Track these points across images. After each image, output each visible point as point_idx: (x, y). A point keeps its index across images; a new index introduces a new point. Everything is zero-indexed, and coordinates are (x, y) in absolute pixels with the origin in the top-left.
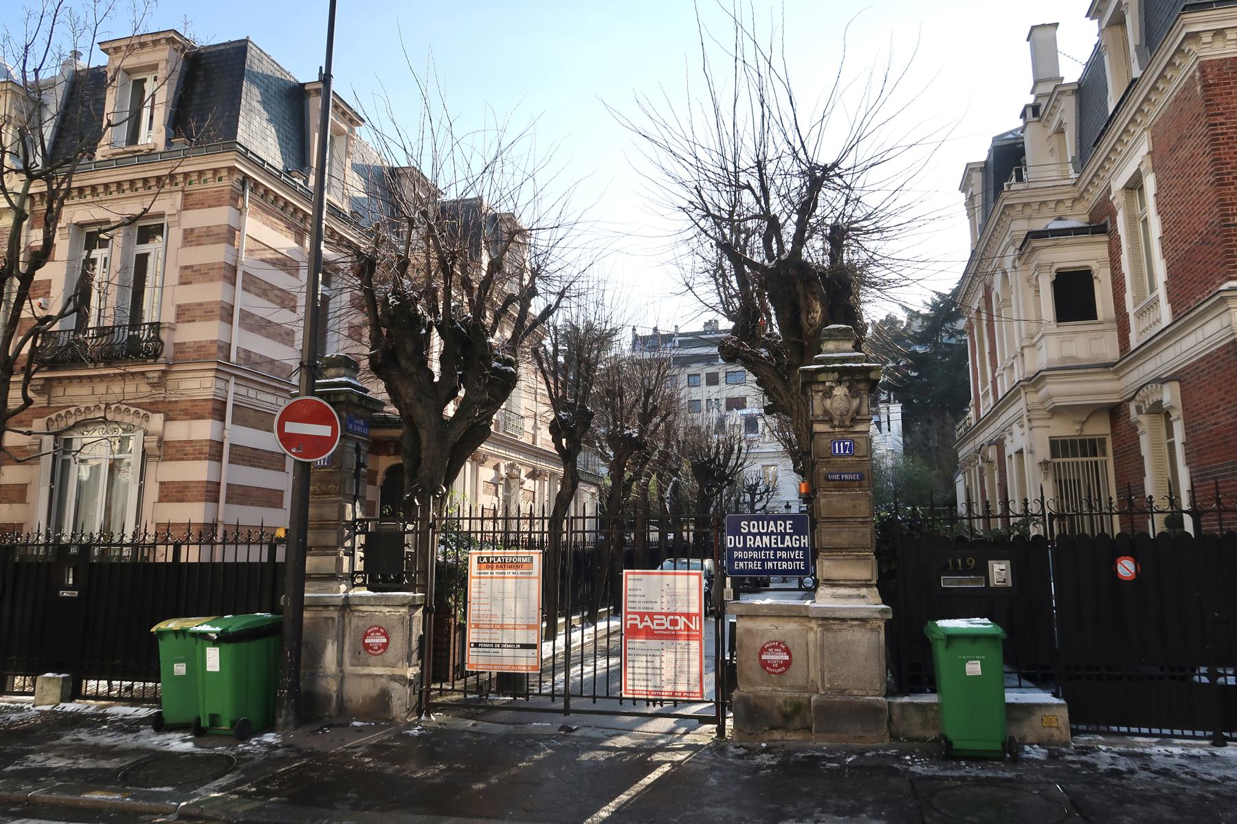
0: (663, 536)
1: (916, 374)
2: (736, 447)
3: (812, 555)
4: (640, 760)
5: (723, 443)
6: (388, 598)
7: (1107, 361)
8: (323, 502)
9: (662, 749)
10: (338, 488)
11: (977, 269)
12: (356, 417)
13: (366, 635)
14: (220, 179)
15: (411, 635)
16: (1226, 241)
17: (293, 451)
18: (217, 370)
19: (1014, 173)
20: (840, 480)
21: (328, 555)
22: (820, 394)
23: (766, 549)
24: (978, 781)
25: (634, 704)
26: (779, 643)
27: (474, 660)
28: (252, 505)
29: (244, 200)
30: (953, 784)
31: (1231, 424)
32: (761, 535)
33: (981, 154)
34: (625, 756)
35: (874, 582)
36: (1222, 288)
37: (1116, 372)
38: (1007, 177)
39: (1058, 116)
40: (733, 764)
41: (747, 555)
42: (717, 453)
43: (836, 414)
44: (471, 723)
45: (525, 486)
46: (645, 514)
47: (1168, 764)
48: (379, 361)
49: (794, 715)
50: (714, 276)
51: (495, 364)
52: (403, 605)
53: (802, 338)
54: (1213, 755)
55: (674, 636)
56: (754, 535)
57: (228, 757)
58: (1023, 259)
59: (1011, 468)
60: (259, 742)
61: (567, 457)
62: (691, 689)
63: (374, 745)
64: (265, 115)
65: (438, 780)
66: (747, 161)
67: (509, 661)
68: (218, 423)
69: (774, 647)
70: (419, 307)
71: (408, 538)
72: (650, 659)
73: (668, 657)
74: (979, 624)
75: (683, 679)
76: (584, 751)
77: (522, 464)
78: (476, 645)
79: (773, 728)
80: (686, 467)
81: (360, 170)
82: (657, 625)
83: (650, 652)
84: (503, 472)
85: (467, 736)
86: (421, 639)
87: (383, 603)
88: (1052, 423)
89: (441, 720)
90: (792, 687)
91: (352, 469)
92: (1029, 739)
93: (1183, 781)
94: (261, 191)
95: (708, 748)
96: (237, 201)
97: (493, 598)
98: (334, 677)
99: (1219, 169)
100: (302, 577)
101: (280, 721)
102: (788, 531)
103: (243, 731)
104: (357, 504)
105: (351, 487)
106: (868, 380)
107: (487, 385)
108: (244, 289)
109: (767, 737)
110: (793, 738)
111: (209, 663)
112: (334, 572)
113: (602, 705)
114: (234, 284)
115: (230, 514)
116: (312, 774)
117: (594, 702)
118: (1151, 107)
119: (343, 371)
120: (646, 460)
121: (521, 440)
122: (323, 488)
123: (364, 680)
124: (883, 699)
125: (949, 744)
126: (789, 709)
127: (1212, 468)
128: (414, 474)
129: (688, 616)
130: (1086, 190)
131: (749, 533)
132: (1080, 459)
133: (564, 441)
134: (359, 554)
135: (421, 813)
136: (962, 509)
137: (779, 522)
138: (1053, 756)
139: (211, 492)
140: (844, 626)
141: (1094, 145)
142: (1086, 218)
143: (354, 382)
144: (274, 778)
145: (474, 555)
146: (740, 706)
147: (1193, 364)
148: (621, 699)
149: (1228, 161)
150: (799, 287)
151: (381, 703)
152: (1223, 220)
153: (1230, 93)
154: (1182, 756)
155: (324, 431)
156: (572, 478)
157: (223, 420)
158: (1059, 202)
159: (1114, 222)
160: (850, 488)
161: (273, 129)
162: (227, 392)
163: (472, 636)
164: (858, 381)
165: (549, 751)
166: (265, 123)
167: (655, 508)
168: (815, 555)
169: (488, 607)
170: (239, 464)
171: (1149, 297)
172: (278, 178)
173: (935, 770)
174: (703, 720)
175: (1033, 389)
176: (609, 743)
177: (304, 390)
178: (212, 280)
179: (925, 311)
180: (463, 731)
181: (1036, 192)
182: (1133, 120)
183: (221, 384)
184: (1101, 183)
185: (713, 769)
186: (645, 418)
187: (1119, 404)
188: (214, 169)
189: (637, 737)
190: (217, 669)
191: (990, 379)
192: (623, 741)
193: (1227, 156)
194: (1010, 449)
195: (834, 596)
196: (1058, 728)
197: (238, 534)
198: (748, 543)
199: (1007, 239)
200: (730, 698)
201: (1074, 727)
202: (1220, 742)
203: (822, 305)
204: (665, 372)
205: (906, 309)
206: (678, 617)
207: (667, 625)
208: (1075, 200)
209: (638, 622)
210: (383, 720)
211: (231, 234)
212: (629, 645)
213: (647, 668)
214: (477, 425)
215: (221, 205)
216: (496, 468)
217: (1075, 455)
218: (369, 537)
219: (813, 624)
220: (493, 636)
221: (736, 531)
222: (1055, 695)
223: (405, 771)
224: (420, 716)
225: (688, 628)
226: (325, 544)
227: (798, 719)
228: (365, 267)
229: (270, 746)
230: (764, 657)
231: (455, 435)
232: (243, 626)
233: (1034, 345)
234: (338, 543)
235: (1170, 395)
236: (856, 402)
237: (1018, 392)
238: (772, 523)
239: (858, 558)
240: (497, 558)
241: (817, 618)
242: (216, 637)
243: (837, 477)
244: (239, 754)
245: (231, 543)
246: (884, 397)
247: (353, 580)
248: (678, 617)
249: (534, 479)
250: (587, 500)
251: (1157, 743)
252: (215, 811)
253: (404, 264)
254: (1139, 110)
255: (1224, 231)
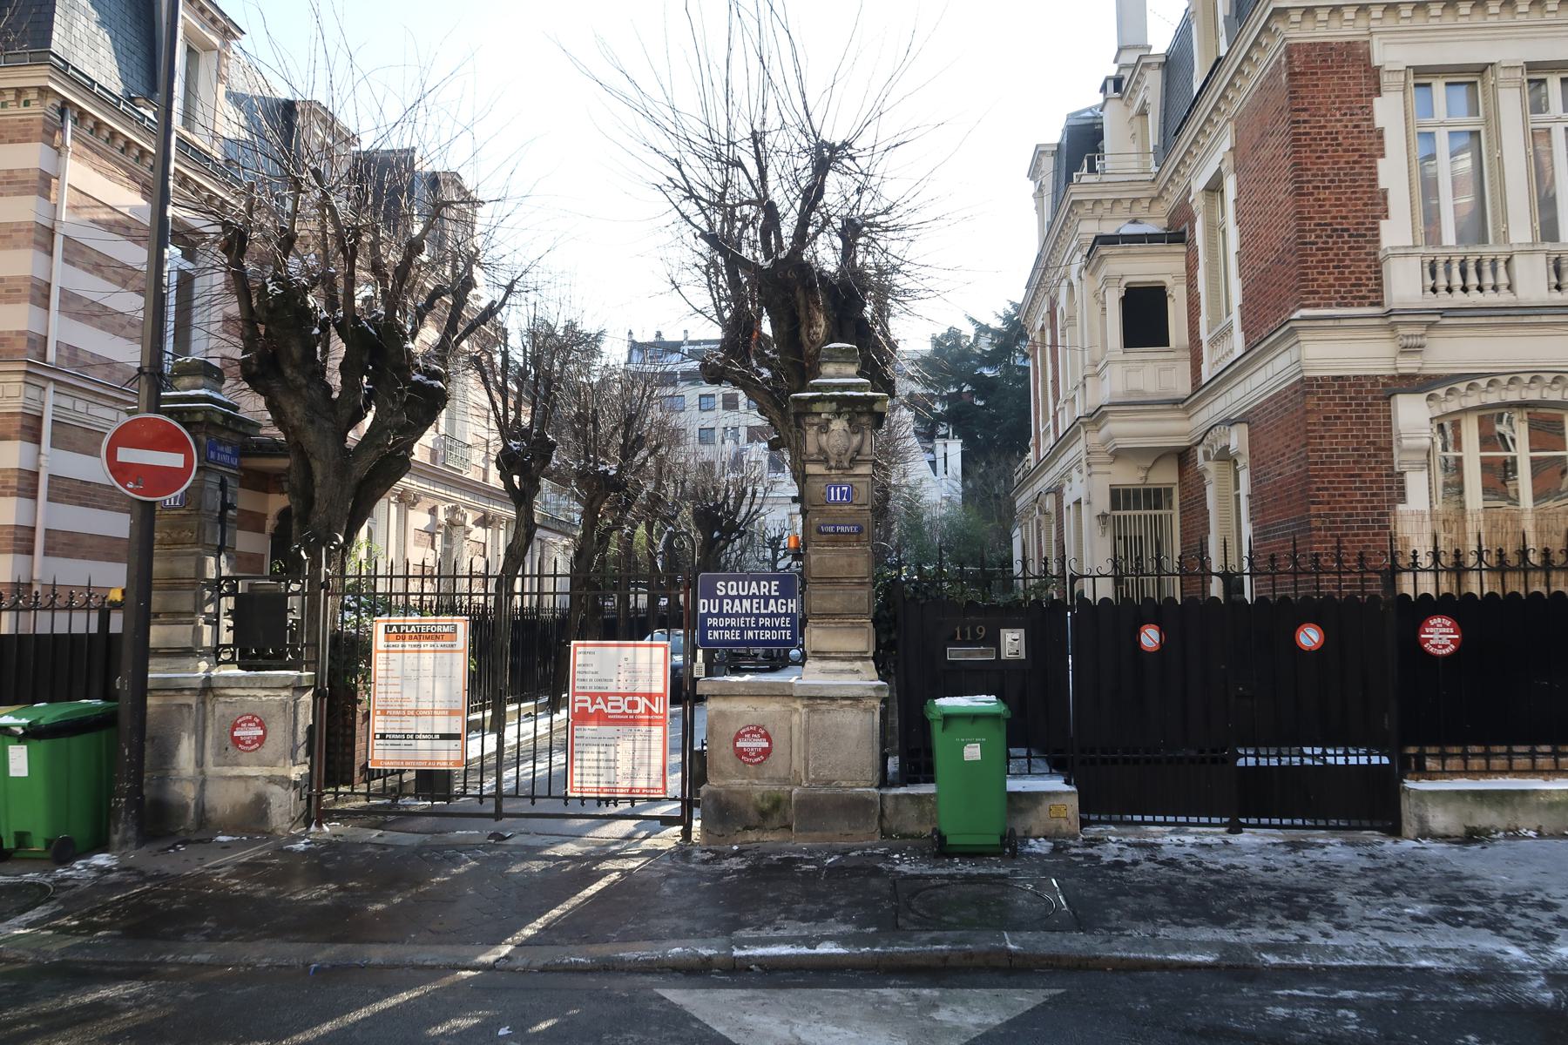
0: (653, 600)
1: (982, 403)
2: (750, 490)
3: (800, 624)
4: (584, 870)
5: (733, 484)
6: (265, 678)
7: (1177, 397)
8: (177, 555)
9: (614, 856)
10: (195, 536)
11: (1042, 278)
12: (220, 442)
13: (235, 726)
14: (27, 103)
15: (296, 725)
16: (1300, 262)
17: (130, 485)
18: (27, 373)
19: (1085, 161)
20: (835, 532)
21: (181, 623)
22: (815, 428)
23: (747, 615)
24: (969, 879)
25: (583, 804)
26: (758, 728)
27: (381, 755)
28: (84, 558)
29: (64, 135)
30: (939, 882)
31: (1295, 475)
32: (741, 598)
33: (1054, 135)
34: (567, 865)
35: (871, 654)
36: (1294, 316)
37: (1186, 410)
38: (1078, 167)
39: (1141, 95)
40: (693, 870)
41: (723, 622)
42: (727, 497)
43: (833, 453)
44: (376, 833)
45: (472, 536)
46: (629, 571)
47: (1177, 853)
48: (254, 368)
49: (772, 812)
50: (707, 273)
51: (417, 377)
52: (285, 687)
53: (801, 357)
54: (1226, 843)
55: (634, 721)
56: (733, 598)
57: (41, 886)
58: (1090, 268)
59: (1069, 518)
60: (86, 866)
61: (522, 499)
62: (652, 784)
63: (244, 864)
64: (95, 15)
65: (325, 902)
66: (742, 131)
67: (426, 756)
68: (31, 447)
69: (751, 732)
70: (310, 298)
71: (293, 602)
72: (602, 749)
73: (625, 747)
74: (984, 702)
75: (643, 773)
76: (516, 863)
77: (467, 507)
78: (383, 736)
79: (747, 828)
80: (686, 514)
81: (237, 99)
82: (612, 707)
83: (602, 742)
84: (442, 517)
85: (369, 849)
86: (310, 730)
87: (258, 685)
88: (1113, 468)
89: (336, 831)
90: (772, 779)
91: (214, 511)
92: (1035, 832)
93: (1186, 871)
94: (90, 123)
95: (670, 853)
96: (53, 136)
97: (404, 678)
98: (191, 780)
99: (1299, 176)
100: (144, 653)
101: (116, 838)
102: (773, 593)
103: (63, 852)
104: (223, 558)
105: (214, 536)
106: (871, 413)
107: (406, 404)
108: (66, 260)
109: (740, 839)
110: (770, 838)
111: (12, 766)
112: (190, 645)
113: (543, 806)
114: (51, 254)
115: (46, 569)
116: (156, 901)
117: (533, 803)
118: (1236, 94)
119: (201, 381)
120: (628, 507)
121: (467, 476)
122: (174, 535)
123: (232, 783)
124: (875, 791)
125: (942, 839)
126: (766, 805)
127: (1273, 525)
128: (304, 520)
129: (650, 697)
130: (1166, 188)
131: (727, 596)
132: (1142, 512)
133: (516, 478)
134: (226, 622)
135: (297, 941)
136: (1017, 568)
137: (762, 583)
138: (1056, 850)
139: (22, 540)
140: (834, 706)
141: (1176, 134)
142: (1165, 222)
143: (216, 396)
144: (104, 909)
145: (379, 626)
146: (709, 803)
147: (1262, 404)
148: (566, 798)
149: (1309, 166)
150: (799, 294)
151: (255, 814)
152: (1299, 237)
153: (1317, 86)
154: (1194, 845)
155: (175, 460)
156: (526, 526)
157: (37, 440)
158: (1135, 200)
159: (1193, 230)
160: (847, 543)
161: (107, 37)
162: (43, 403)
163: (378, 724)
164: (860, 414)
165: (473, 863)
166: (94, 27)
167: (645, 568)
168: (804, 623)
169: (398, 689)
170: (63, 502)
171: (1225, 321)
172: (115, 107)
173: (925, 869)
174: (667, 821)
175: (1094, 427)
176: (549, 852)
177: (144, 406)
178: (16, 247)
179: (997, 324)
180: (365, 844)
181: (1109, 187)
182: (1216, 108)
183: (33, 392)
184: (1182, 182)
185: (670, 876)
186: (628, 451)
187: (1189, 448)
188: (17, 89)
189: (586, 844)
190: (25, 774)
191: (1051, 413)
192: (570, 848)
193: (1308, 161)
194: (1068, 500)
195: (823, 671)
196: (1066, 818)
197: (55, 596)
198: (725, 608)
199: (1074, 243)
200: (698, 794)
201: (1085, 816)
202: (1235, 829)
203: (827, 318)
204: (652, 392)
205: (974, 321)
206: (637, 698)
207: (624, 708)
208: (1153, 200)
209: (588, 705)
210: (259, 833)
211: (44, 183)
212: (576, 733)
213: (598, 760)
214: (392, 455)
215: (29, 141)
216: (433, 511)
217: (1137, 507)
218: (240, 599)
219: (798, 705)
220: (404, 725)
221: (711, 594)
222: (1067, 782)
223: (283, 892)
224: (308, 826)
225: (649, 712)
226: (177, 609)
227: (776, 816)
228: (236, 242)
229: (102, 870)
230: (739, 744)
231: (360, 469)
232: (61, 716)
233: (1097, 374)
234: (195, 607)
235: (1237, 439)
236: (856, 439)
237: (1077, 431)
238: (754, 584)
239: (853, 626)
240: (410, 627)
241: (802, 698)
242: (21, 732)
243: (831, 529)
244: (57, 881)
245: (44, 609)
246: (942, 431)
247: (218, 656)
248: (637, 698)
249: (485, 527)
250: (557, 554)
251: (1172, 832)
252: (20, 952)
253: (288, 241)
254: (1223, 96)
255: (1299, 250)
